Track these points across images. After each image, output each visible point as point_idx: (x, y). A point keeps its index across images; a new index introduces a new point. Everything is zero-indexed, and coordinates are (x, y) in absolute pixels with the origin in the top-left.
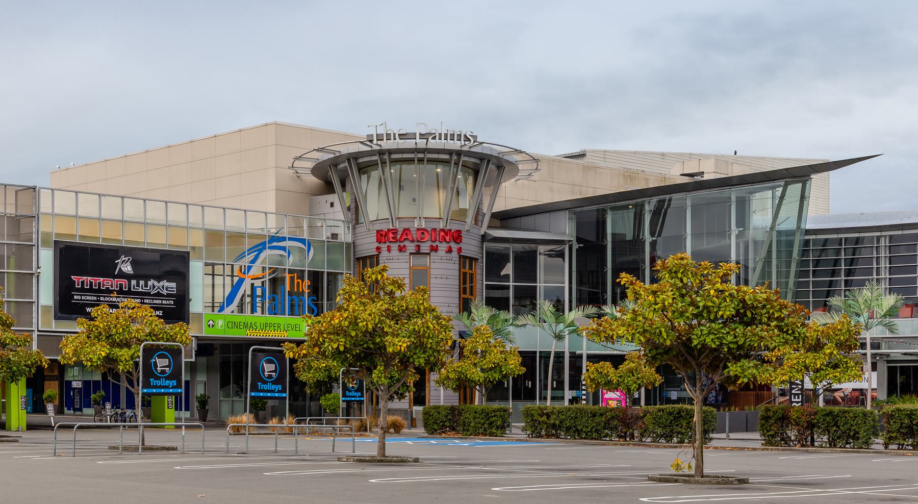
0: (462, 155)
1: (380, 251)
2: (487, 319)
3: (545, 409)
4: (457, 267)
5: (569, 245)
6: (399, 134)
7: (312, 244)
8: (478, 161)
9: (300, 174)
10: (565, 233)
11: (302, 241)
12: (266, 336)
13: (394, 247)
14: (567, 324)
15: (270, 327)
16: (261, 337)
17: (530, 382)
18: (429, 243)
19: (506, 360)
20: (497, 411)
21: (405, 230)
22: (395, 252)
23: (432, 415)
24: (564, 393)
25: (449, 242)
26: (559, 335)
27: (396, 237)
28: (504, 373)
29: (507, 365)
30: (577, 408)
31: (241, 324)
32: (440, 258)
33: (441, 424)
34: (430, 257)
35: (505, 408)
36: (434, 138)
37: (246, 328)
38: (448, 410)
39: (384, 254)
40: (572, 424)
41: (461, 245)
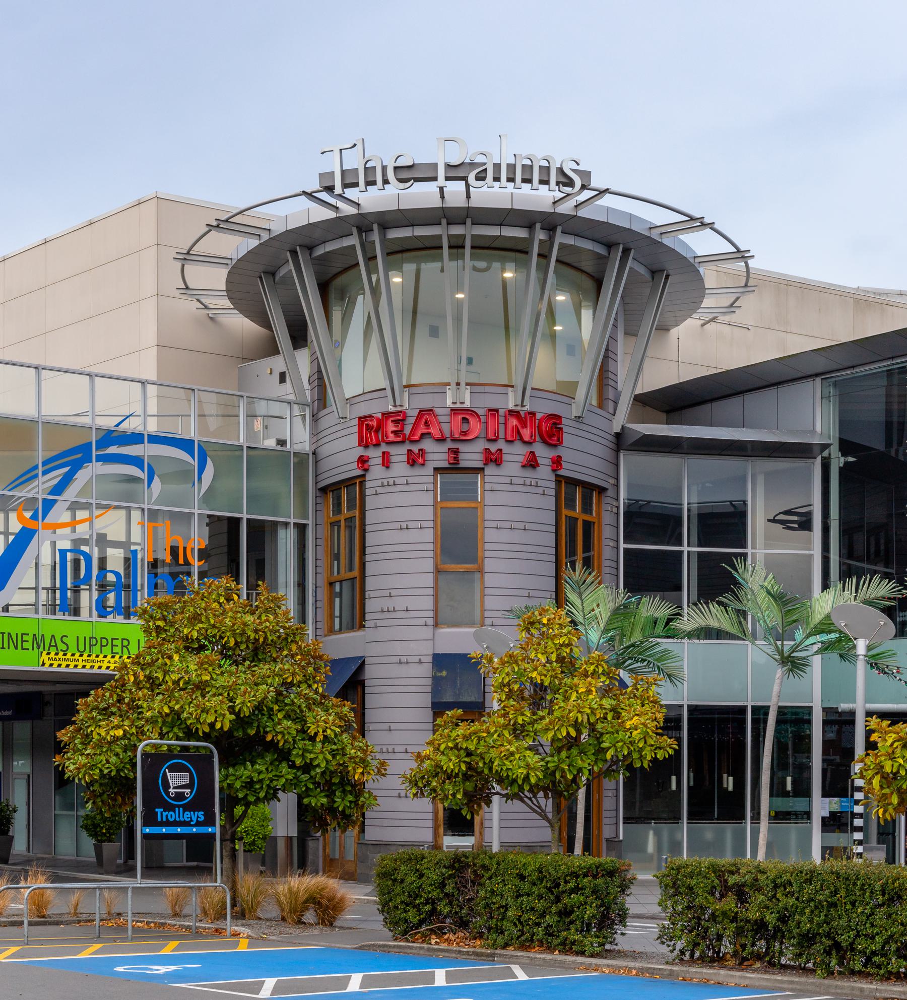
0: (559, 229)
1: (366, 466)
2: (605, 618)
3: (732, 873)
4: (551, 502)
5: (823, 459)
6: (395, 168)
7: (209, 453)
8: (600, 250)
9: (214, 311)
10: (813, 431)
11: (186, 445)
12: (92, 667)
13: (399, 453)
14: (812, 625)
15: (102, 646)
16: (79, 670)
17: (731, 779)
18: (480, 446)
19: (617, 716)
20: (585, 875)
21: (422, 413)
22: (400, 467)
23: (402, 881)
24: (810, 804)
25: (530, 443)
26: (789, 656)
27: (402, 430)
28: (608, 756)
29: (617, 732)
30: (838, 875)
31: (25, 638)
32: (508, 480)
33: (428, 908)
34: (483, 476)
35: (609, 866)
36: (481, 177)
37: (39, 648)
38: (445, 867)
39: (376, 471)
40: (819, 925)
41: (561, 451)
